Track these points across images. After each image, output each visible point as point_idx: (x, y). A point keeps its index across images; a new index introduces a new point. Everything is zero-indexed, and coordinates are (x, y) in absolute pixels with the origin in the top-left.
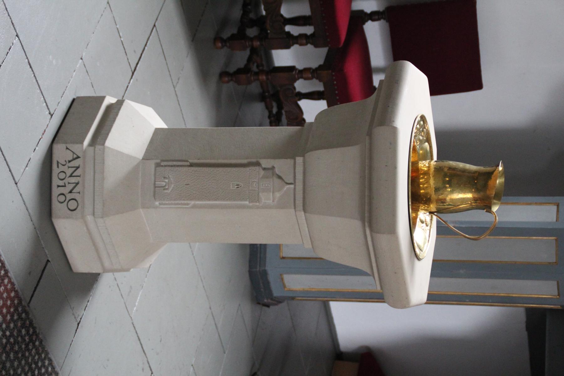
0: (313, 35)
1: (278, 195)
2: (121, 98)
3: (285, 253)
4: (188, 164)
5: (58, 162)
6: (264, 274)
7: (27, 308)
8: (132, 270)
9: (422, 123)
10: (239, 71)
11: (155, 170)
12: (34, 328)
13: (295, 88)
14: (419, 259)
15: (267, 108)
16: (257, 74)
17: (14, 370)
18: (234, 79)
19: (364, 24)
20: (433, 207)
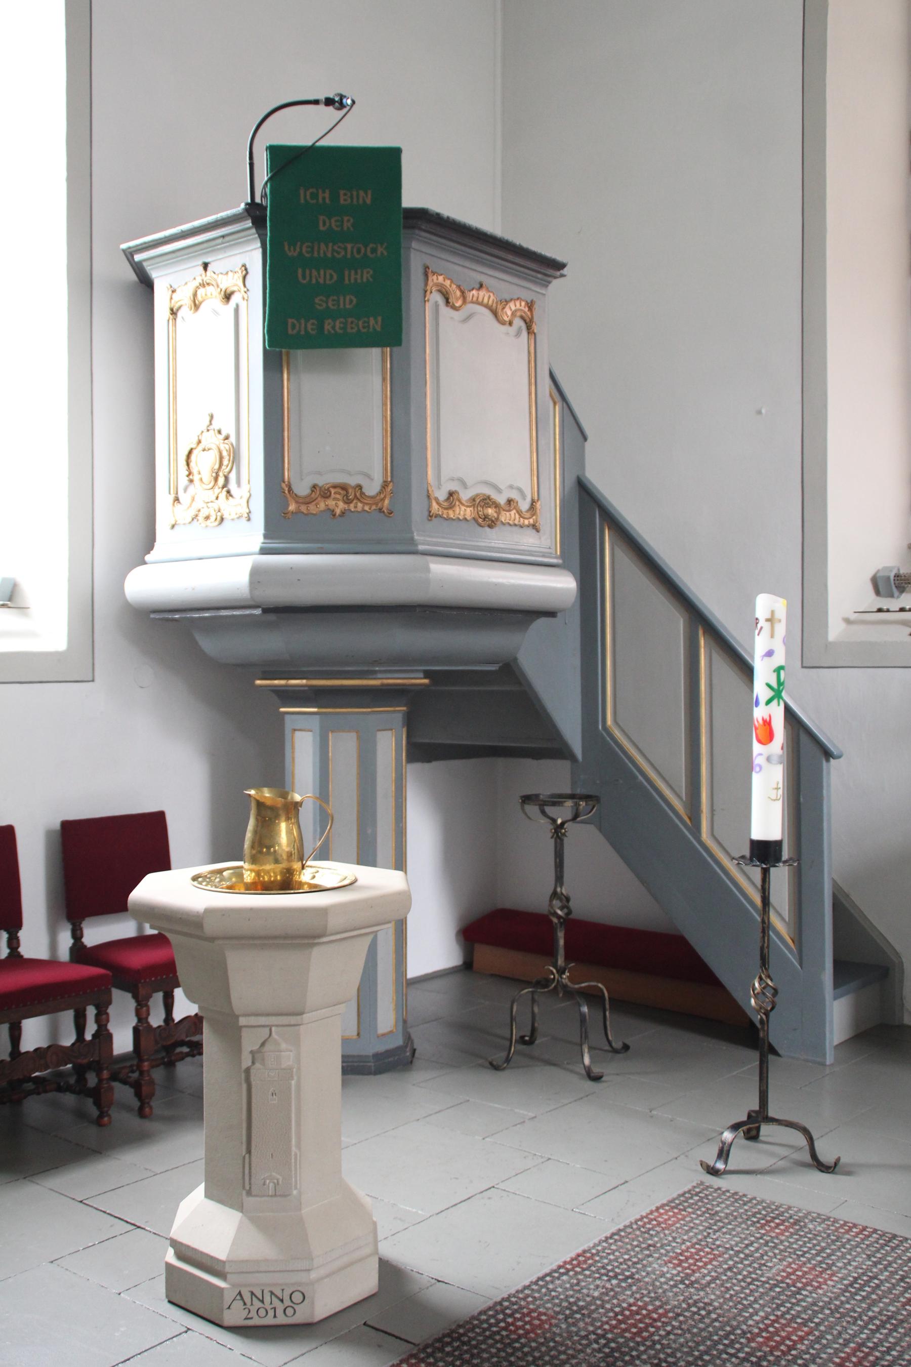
0: (97, 1007)
1: (284, 1046)
2: (168, 1242)
3: (352, 1032)
4: (247, 1156)
5: (246, 1319)
6: (377, 1056)
7: (421, 1347)
8: (374, 1219)
9: (200, 879)
10: (138, 1095)
11: (256, 1196)
12: (444, 1336)
13: (159, 1027)
14: (356, 881)
15: (182, 1059)
16: (142, 1073)
17: (493, 1357)
18: (147, 1101)
19: (86, 946)
20: (297, 865)
